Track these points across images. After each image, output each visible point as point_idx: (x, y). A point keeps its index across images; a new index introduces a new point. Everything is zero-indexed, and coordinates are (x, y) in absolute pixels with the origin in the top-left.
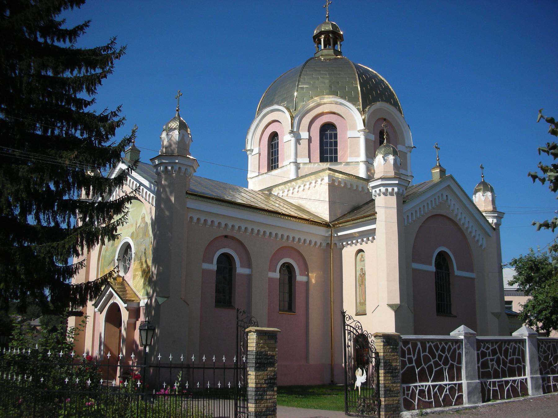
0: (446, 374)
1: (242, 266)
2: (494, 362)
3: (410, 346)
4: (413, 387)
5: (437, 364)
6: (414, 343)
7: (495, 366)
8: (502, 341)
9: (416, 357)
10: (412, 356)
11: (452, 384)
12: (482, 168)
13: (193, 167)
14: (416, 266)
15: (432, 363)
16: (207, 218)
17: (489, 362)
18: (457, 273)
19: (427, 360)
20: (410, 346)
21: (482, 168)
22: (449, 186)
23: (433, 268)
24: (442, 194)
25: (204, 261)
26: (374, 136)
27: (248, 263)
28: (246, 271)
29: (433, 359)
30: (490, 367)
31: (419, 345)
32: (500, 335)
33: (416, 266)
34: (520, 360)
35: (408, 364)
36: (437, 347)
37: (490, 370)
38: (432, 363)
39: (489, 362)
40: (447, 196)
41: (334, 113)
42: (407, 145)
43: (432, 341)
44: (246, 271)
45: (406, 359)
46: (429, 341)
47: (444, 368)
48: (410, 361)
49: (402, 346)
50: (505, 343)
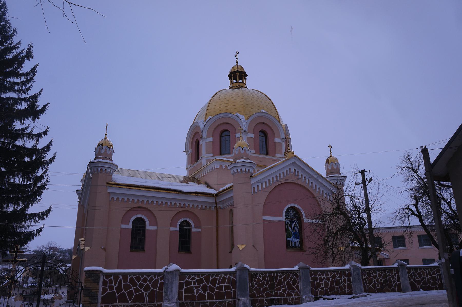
0: (146, 297)
1: (150, 225)
2: (200, 289)
3: (112, 278)
4: (111, 306)
5: (137, 290)
6: (116, 275)
7: (201, 291)
8: (209, 273)
9: (117, 285)
10: (113, 285)
11: (151, 304)
12: (330, 147)
13: (92, 167)
14: (265, 218)
15: (132, 289)
16: (124, 197)
17: (194, 288)
18: (306, 220)
19: (127, 287)
20: (112, 278)
21: (330, 147)
22: (294, 162)
23: (283, 219)
24: (290, 169)
25: (263, 215)
26: (253, 135)
27: (154, 222)
28: (154, 228)
29: (133, 287)
30: (195, 292)
31: (121, 277)
32: (265, 268)
33: (265, 218)
34: (230, 287)
35: (108, 290)
36: (138, 279)
37: (195, 294)
38: (132, 289)
39: (194, 288)
40: (294, 169)
41: (228, 123)
42: (281, 138)
43: (134, 274)
44: (154, 228)
45: (108, 287)
46: (130, 274)
47: (144, 293)
48: (111, 288)
49: (105, 278)
50: (213, 275)
